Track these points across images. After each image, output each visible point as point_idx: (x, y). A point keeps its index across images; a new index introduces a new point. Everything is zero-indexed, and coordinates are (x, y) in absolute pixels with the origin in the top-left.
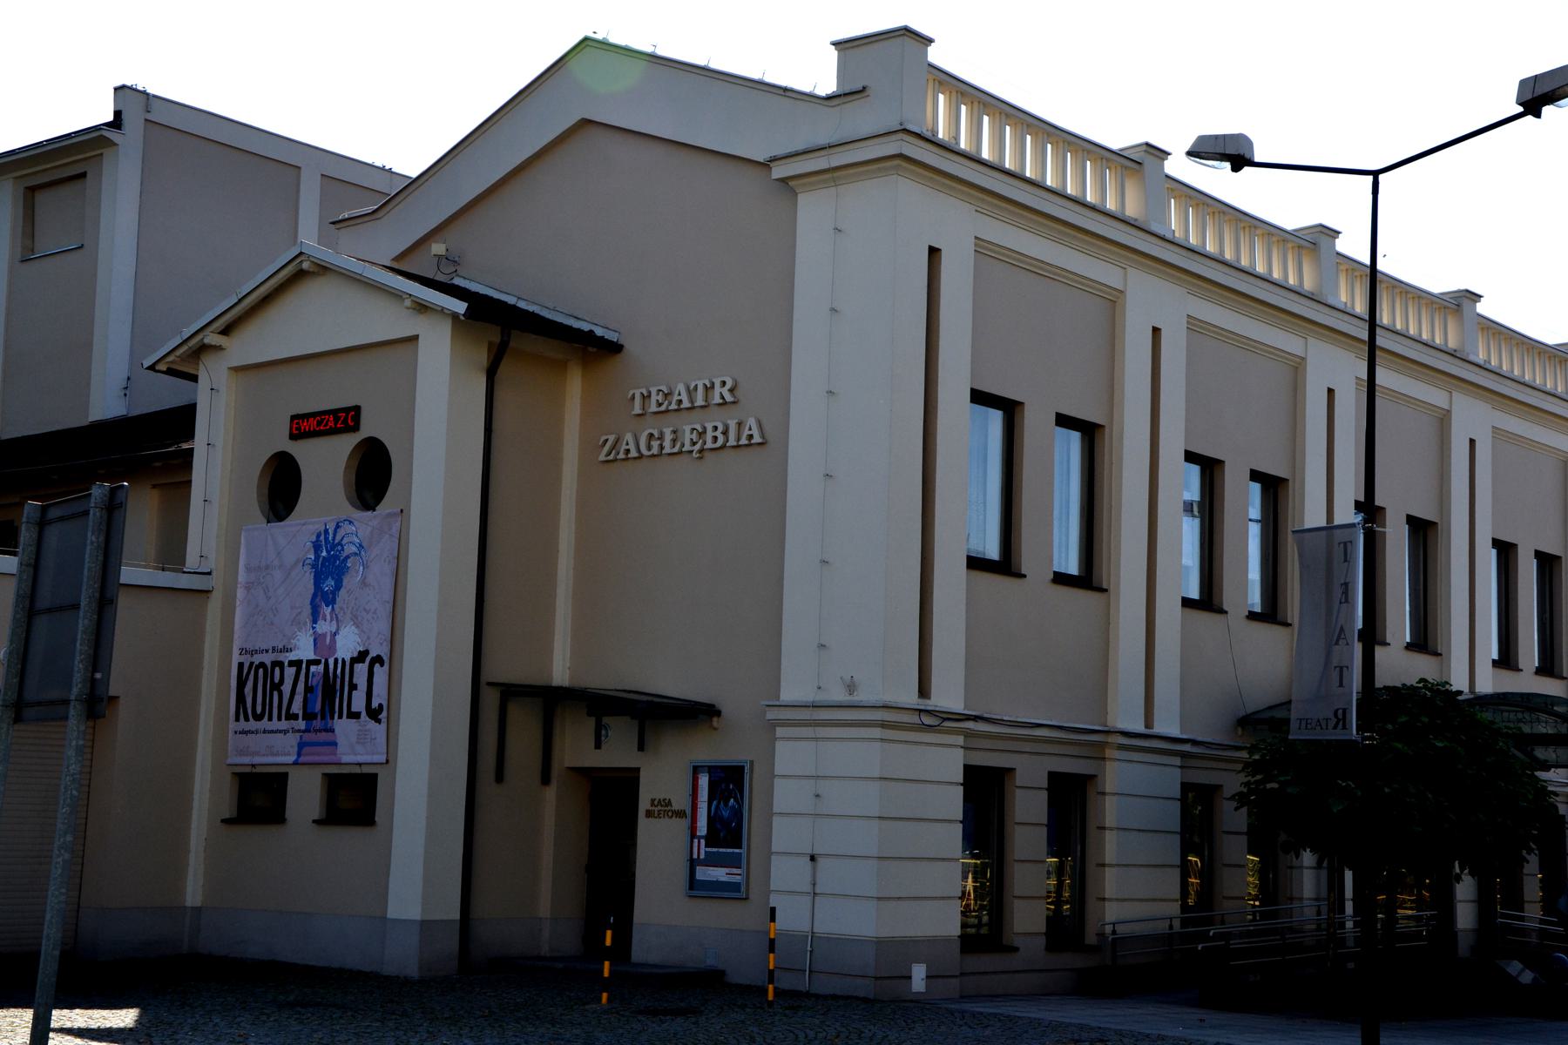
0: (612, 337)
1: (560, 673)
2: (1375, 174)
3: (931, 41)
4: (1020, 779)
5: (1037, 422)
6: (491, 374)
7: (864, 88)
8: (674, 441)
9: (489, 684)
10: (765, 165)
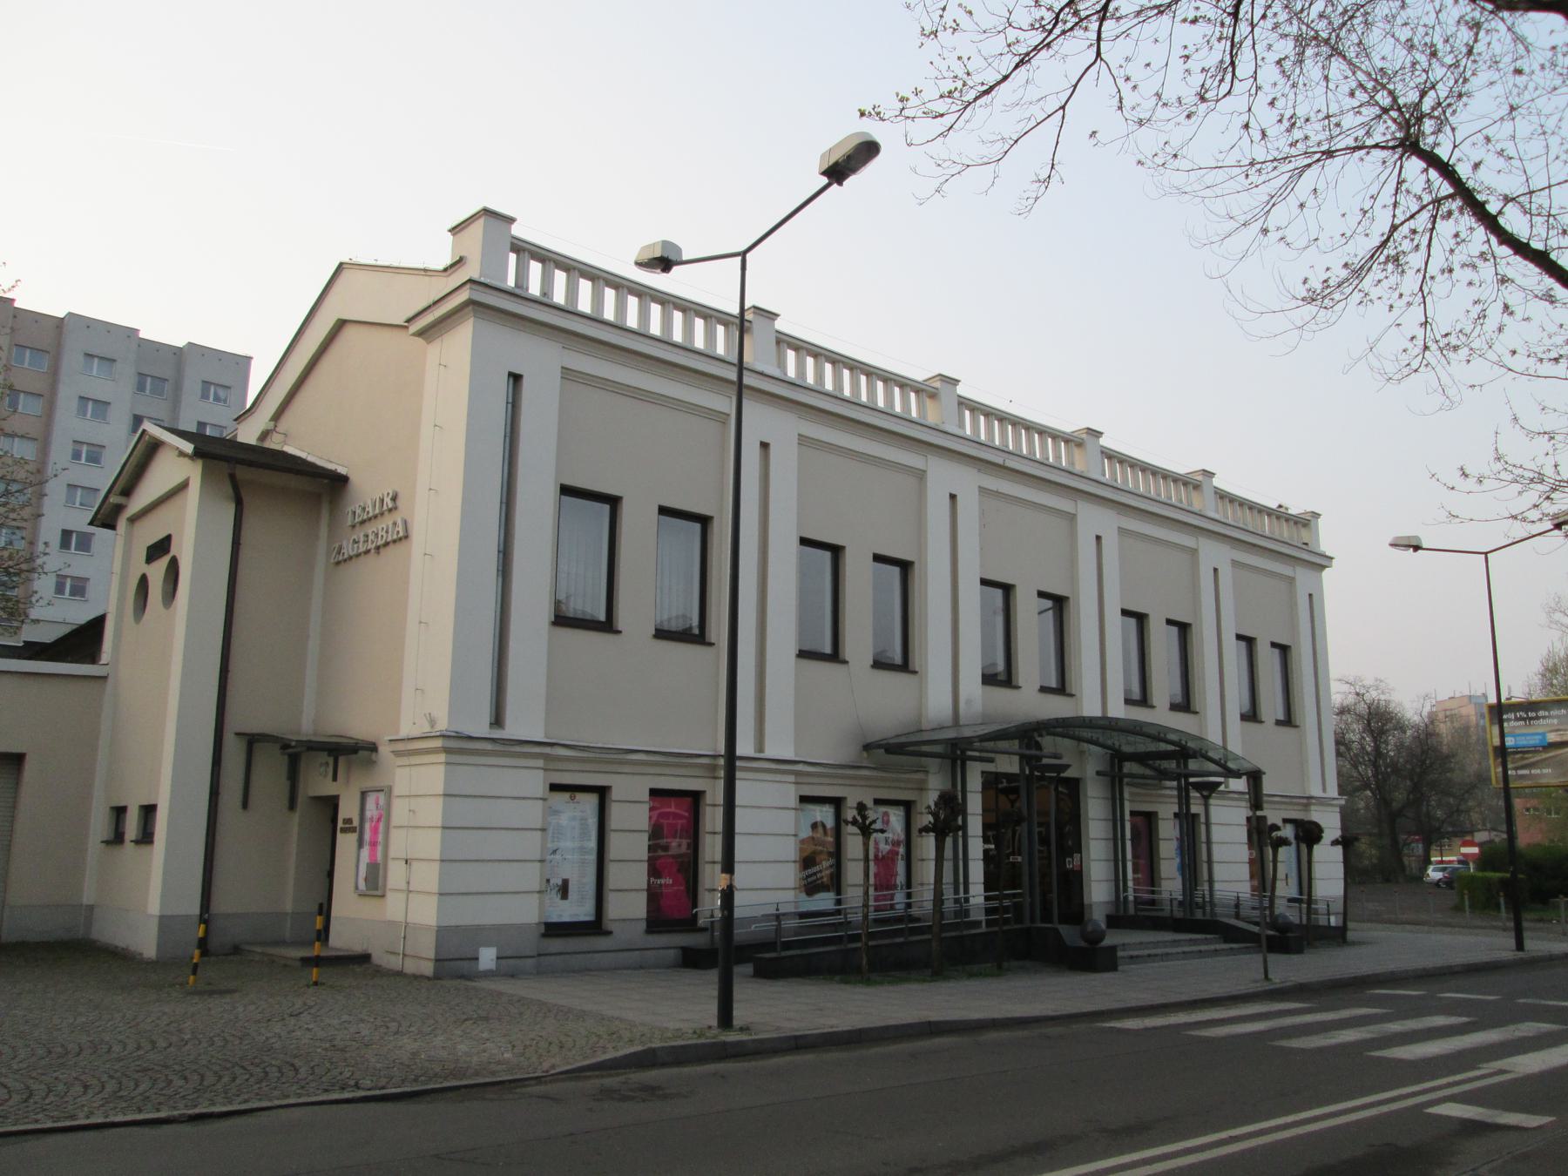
1: (307, 726)
2: (743, 254)
3: (777, 315)
4: (708, 799)
5: (638, 521)
6: (239, 503)
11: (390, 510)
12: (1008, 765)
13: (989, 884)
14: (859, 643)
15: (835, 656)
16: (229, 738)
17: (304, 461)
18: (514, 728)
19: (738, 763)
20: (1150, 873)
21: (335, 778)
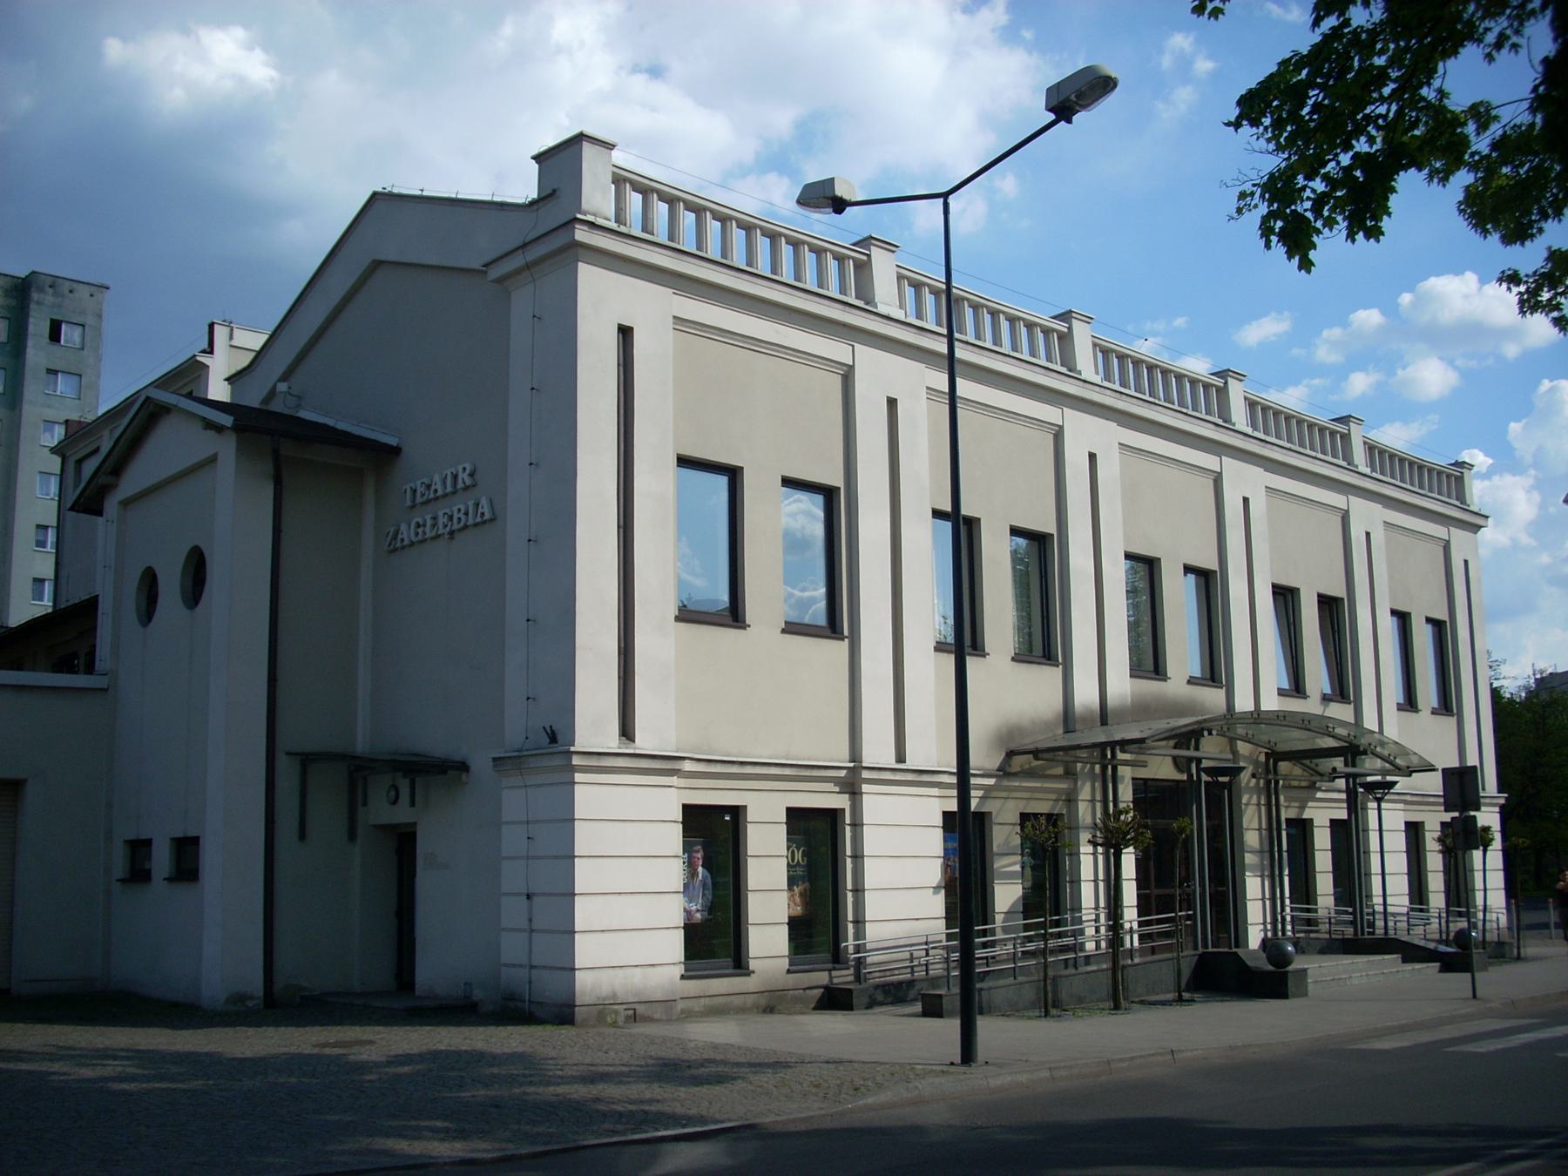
0: (393, 441)
1: (362, 743)
2: (945, 196)
6: (278, 483)
7: (554, 191)
8: (434, 526)
9: (289, 754)
10: (480, 273)
11: (466, 488)
12: (1162, 768)
13: (1143, 907)
14: (768, 594)
15: (735, 615)
16: (282, 762)
17: (333, 429)
18: (645, 741)
19: (954, 780)
20: (1304, 891)
21: (413, 804)
